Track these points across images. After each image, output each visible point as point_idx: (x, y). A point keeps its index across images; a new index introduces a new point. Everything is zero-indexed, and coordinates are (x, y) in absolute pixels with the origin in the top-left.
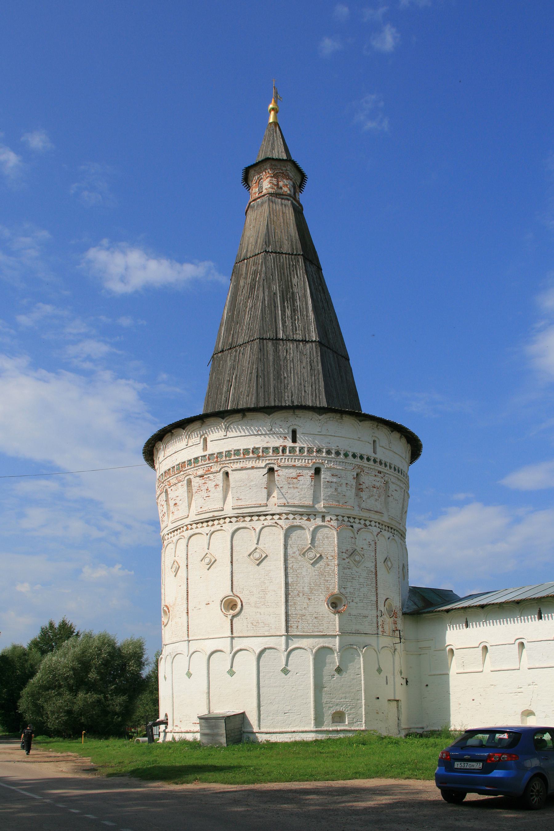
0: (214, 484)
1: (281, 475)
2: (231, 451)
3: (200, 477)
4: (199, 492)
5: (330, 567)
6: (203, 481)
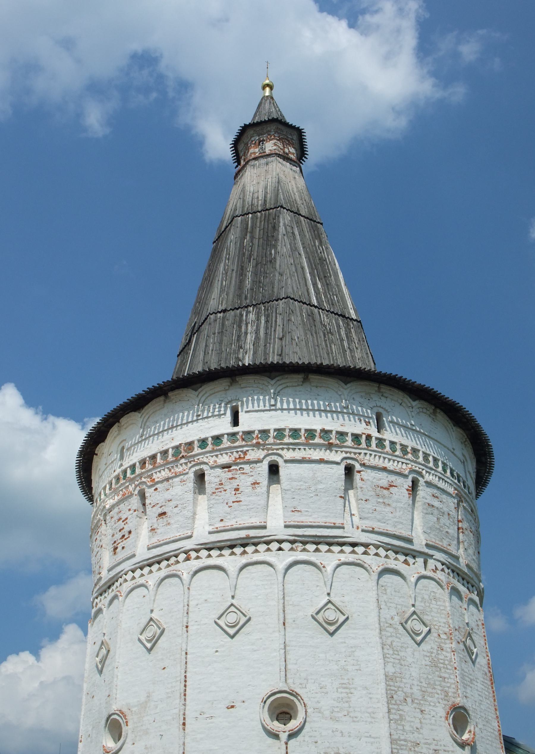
0: (251, 480)
2: (284, 430)
3: (223, 468)
4: (219, 494)
5: (444, 653)
6: (230, 475)
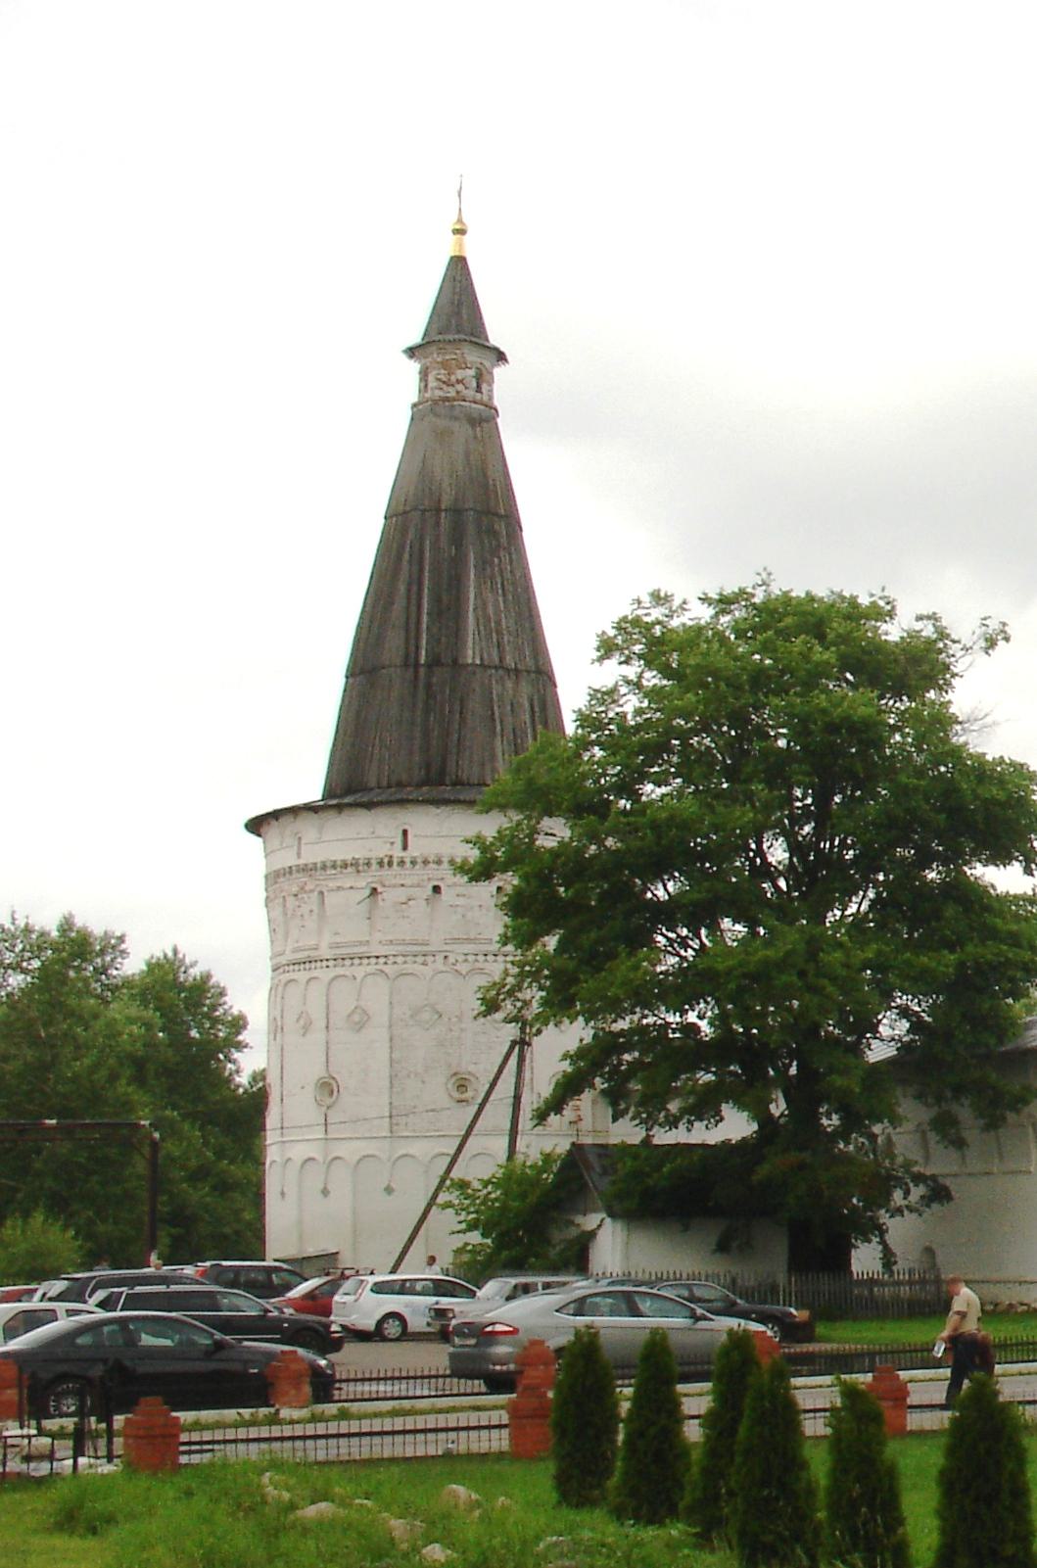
1: (389, 896)
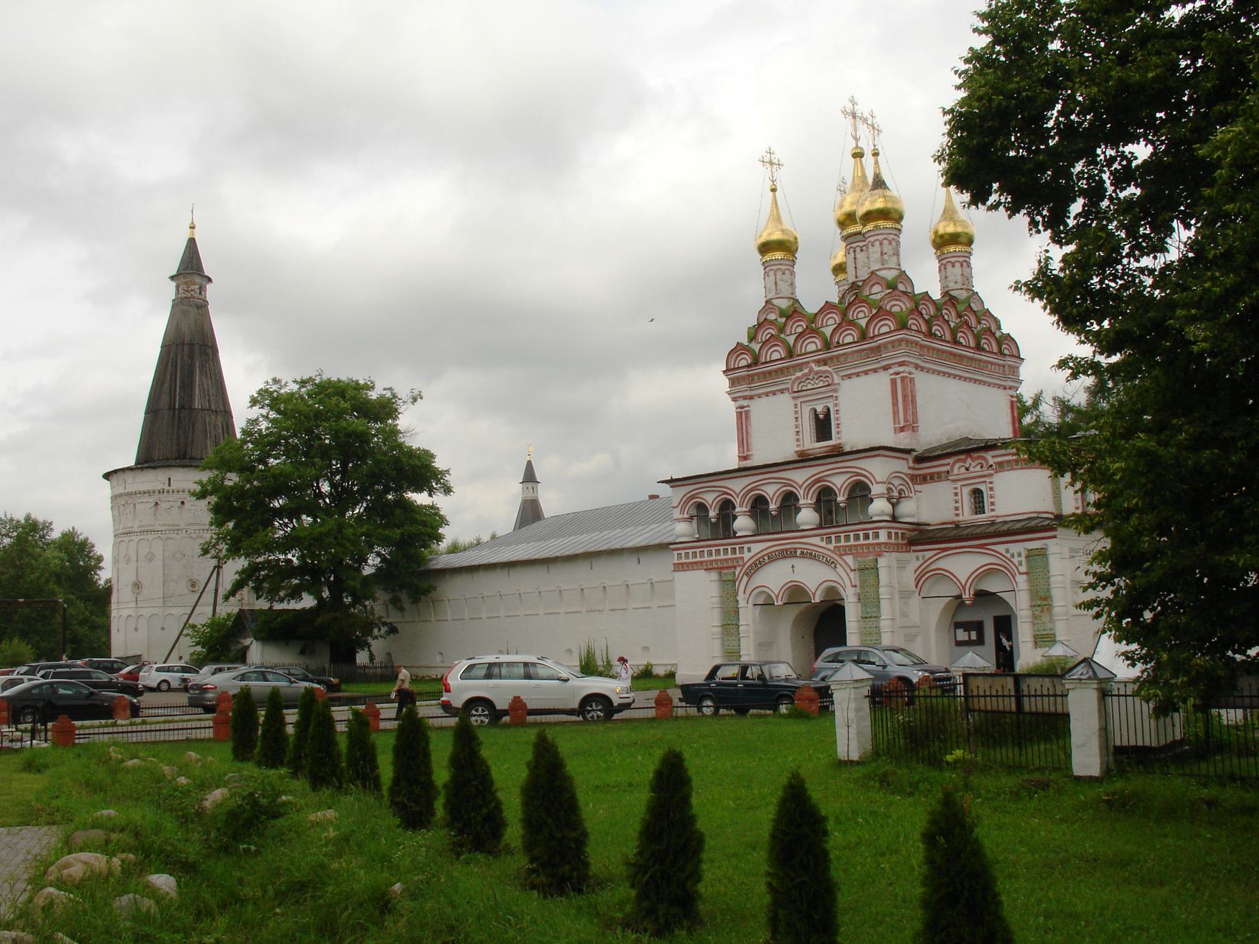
1: (163, 506)
